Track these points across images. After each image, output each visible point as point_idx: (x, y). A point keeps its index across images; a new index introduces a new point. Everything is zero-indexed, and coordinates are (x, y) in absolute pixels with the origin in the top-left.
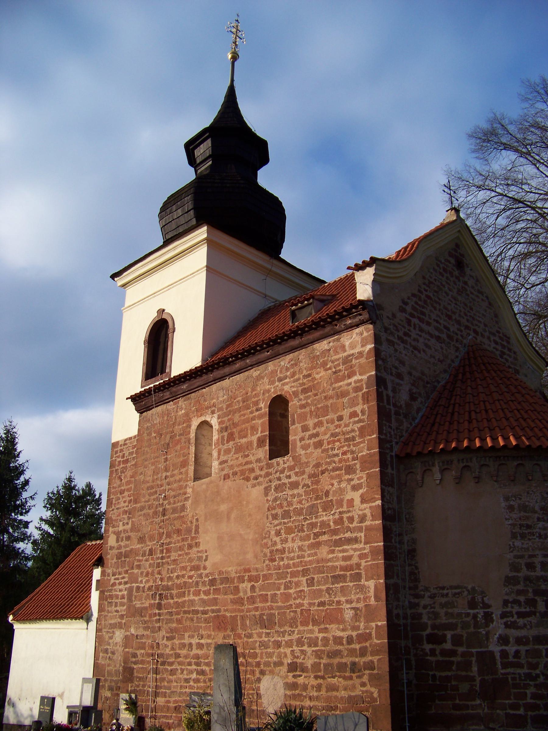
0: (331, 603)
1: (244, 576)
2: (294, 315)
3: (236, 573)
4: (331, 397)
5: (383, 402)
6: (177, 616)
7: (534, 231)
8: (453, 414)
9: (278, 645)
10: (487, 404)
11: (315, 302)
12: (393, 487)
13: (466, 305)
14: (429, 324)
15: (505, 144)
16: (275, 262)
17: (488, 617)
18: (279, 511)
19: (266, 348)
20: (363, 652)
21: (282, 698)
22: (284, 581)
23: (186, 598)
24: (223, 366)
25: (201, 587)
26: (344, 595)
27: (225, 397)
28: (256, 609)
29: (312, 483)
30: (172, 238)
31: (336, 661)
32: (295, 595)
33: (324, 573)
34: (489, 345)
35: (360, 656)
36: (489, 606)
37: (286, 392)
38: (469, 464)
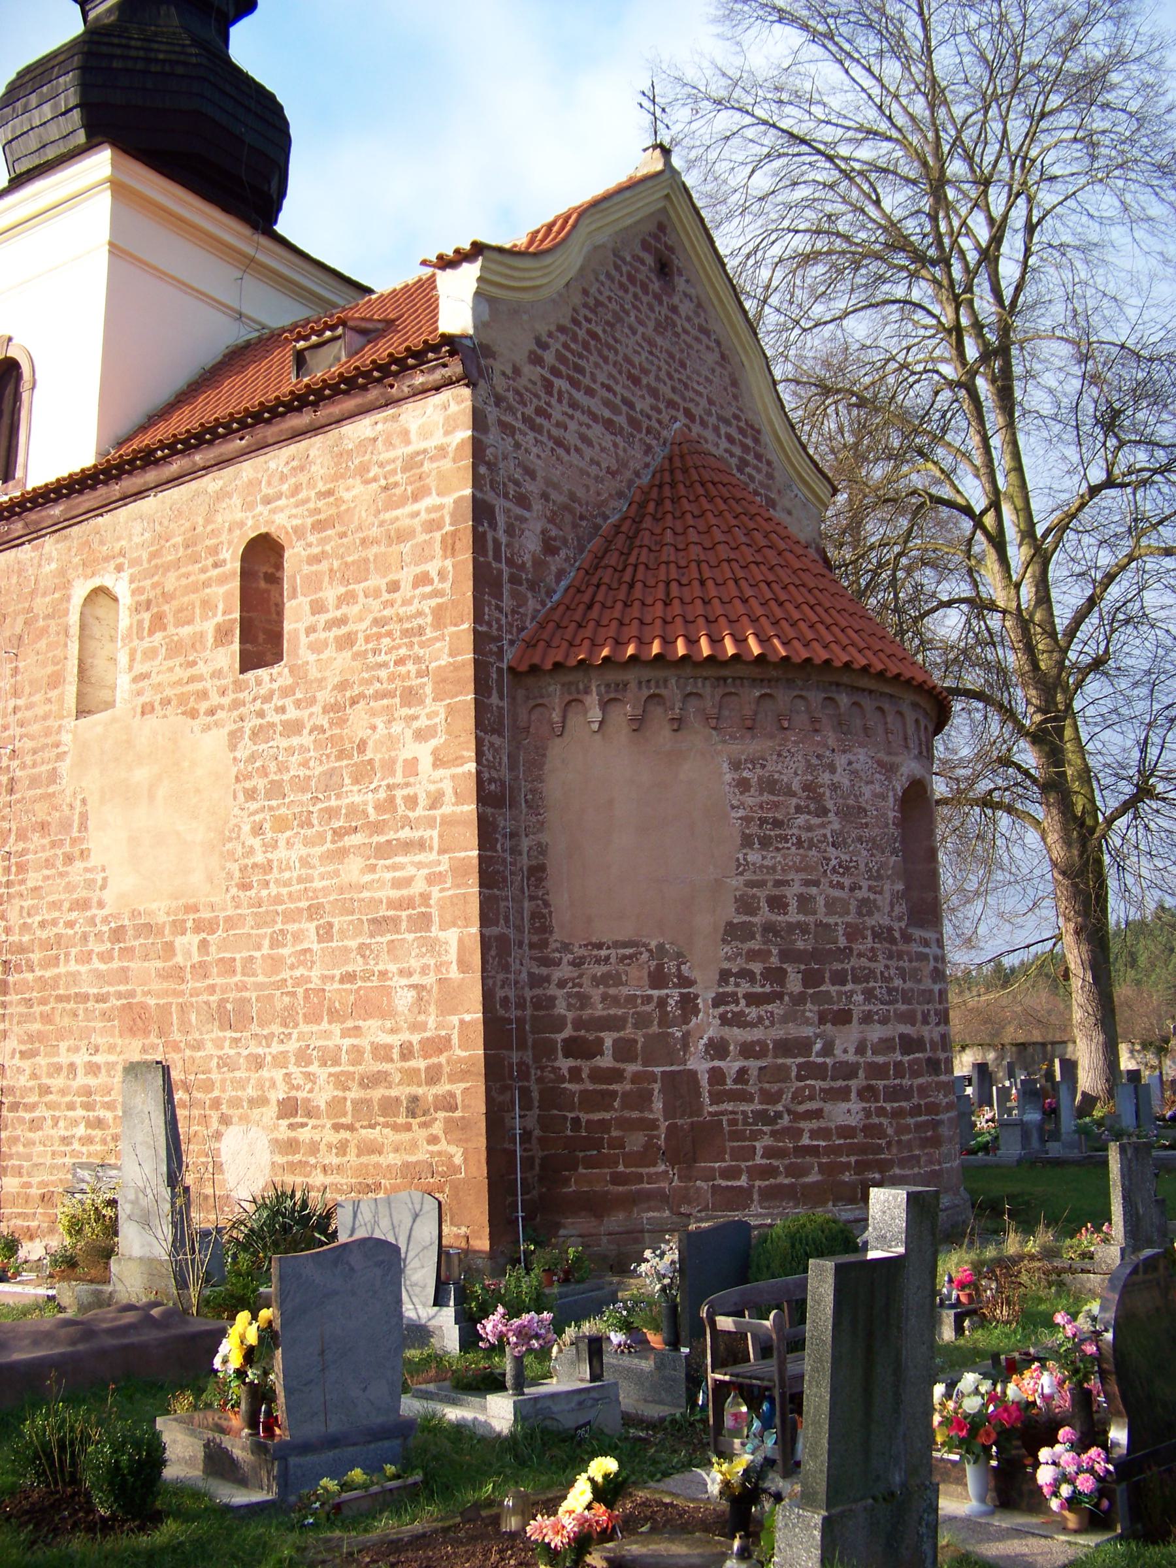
0: (368, 975)
1: (184, 921)
2: (300, 360)
3: (168, 914)
4: (376, 541)
5: (485, 555)
6: (42, 1008)
7: (829, 208)
8: (631, 586)
9: (257, 1063)
10: (704, 566)
11: (349, 334)
12: (500, 734)
13: (671, 356)
14: (590, 392)
15: (780, 10)
16: (264, 241)
17: (688, 1005)
18: (261, 783)
19: (238, 430)
20: (433, 1075)
21: (267, 1171)
22: (270, 931)
23: (62, 969)
24: (143, 468)
25: (92, 945)
26: (395, 959)
27: (147, 535)
28: (212, 989)
29: (331, 724)
30: (29, 171)
31: (377, 1093)
32: (293, 959)
33: (352, 913)
34: (717, 445)
35: (427, 1084)
36: (690, 983)
37: (278, 527)
38: (663, 692)
